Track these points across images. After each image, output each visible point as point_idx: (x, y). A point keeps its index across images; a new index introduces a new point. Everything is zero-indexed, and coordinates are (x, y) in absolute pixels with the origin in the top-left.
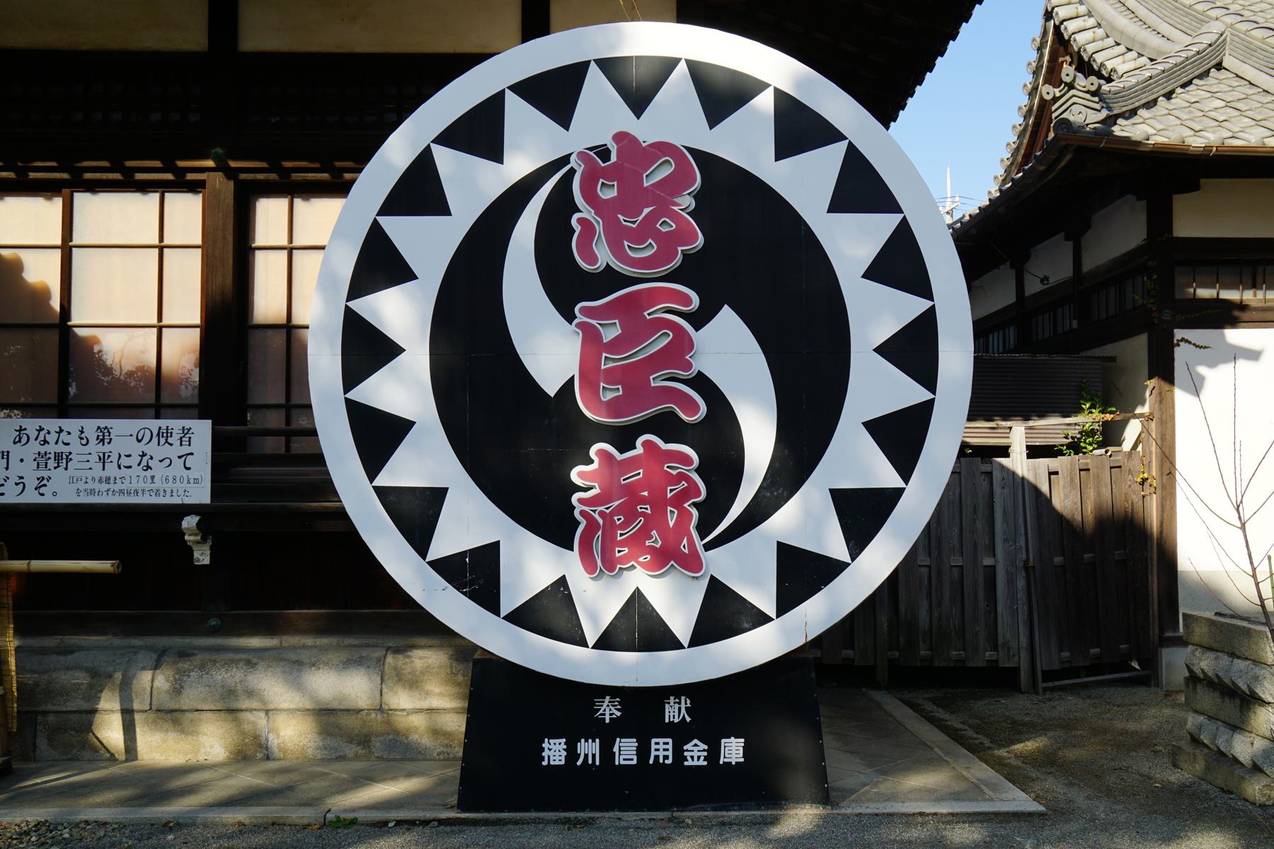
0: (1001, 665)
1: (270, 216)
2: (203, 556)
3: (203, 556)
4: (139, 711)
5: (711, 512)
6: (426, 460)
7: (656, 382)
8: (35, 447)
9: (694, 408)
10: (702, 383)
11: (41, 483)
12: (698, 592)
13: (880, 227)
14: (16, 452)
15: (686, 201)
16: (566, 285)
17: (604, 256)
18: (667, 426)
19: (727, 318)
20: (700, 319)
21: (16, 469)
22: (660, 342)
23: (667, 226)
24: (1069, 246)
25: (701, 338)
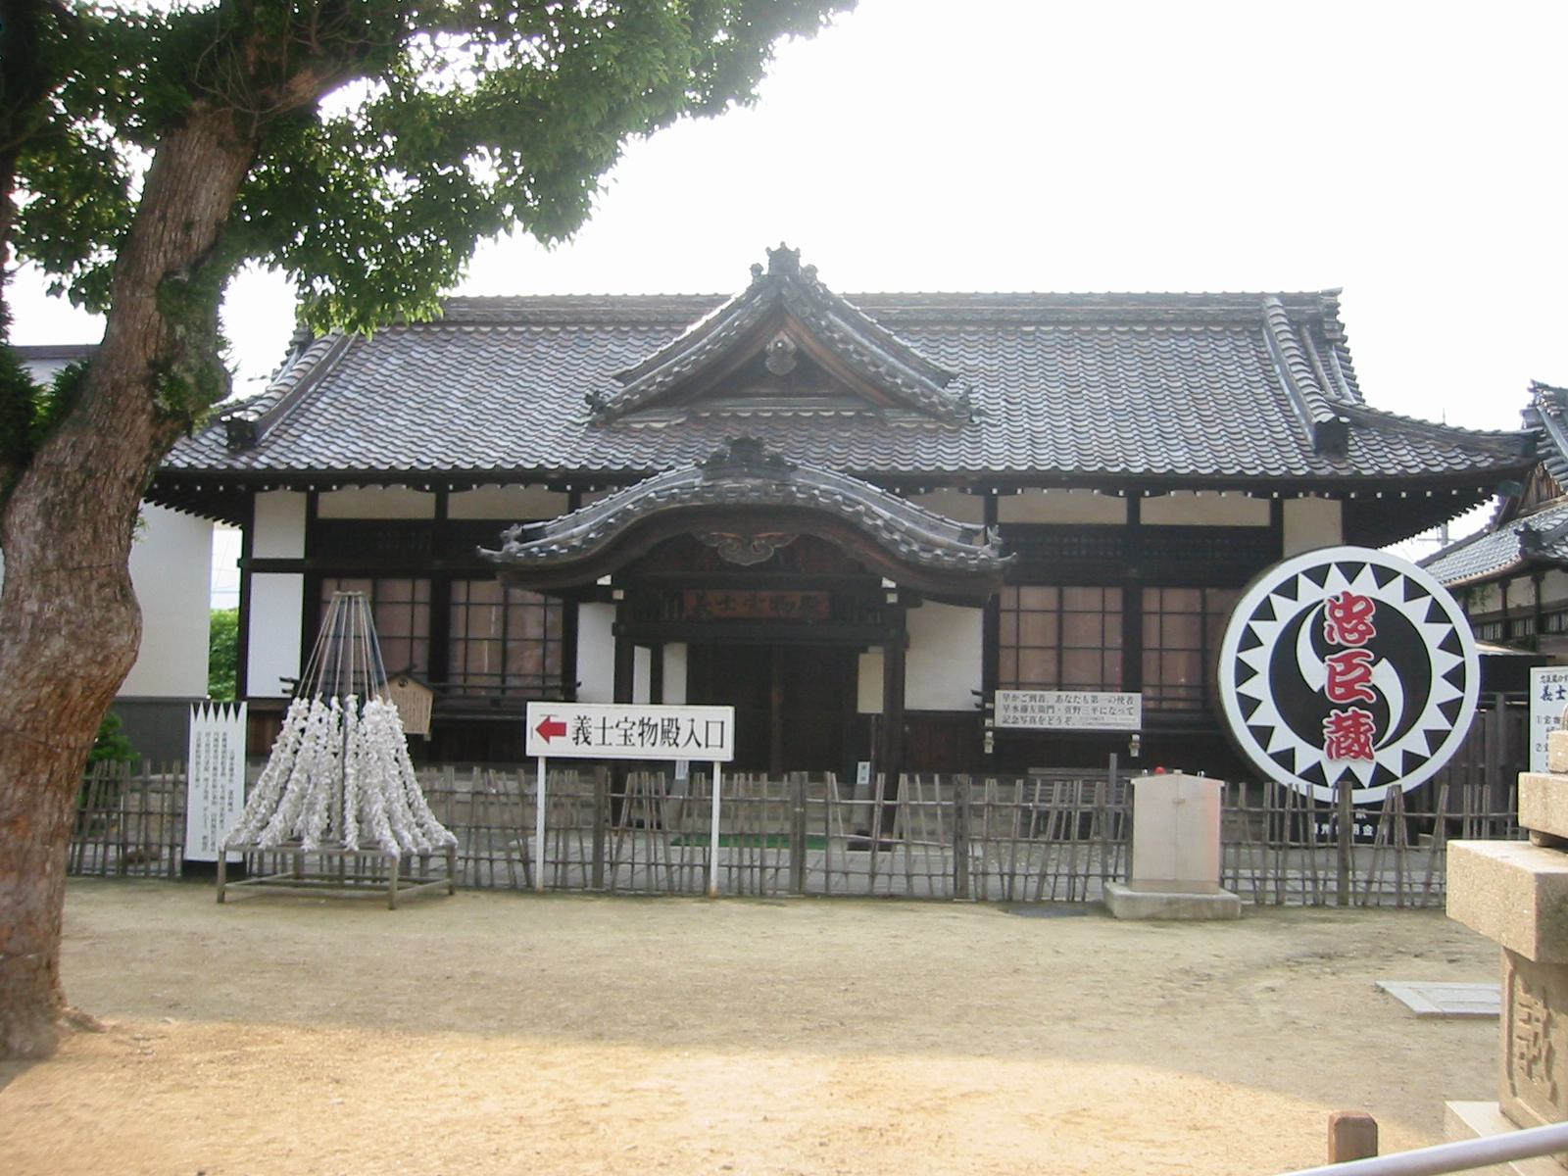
0: (1522, 776)
1: (1151, 599)
2: (989, 750)
3: (989, 750)
4: (873, 858)
5: (1377, 738)
6: (1268, 714)
7: (1357, 687)
8: (1066, 704)
9: (1371, 698)
10: (1374, 688)
11: (1068, 719)
12: (1373, 766)
13: (1399, 582)
14: (1057, 705)
15: (1369, 619)
16: (1322, 649)
17: (1337, 639)
18: (1361, 704)
19: (1384, 661)
20: (1374, 664)
21: (1057, 713)
22: (1358, 672)
23: (1361, 627)
24: (1500, 591)
25: (1373, 670)
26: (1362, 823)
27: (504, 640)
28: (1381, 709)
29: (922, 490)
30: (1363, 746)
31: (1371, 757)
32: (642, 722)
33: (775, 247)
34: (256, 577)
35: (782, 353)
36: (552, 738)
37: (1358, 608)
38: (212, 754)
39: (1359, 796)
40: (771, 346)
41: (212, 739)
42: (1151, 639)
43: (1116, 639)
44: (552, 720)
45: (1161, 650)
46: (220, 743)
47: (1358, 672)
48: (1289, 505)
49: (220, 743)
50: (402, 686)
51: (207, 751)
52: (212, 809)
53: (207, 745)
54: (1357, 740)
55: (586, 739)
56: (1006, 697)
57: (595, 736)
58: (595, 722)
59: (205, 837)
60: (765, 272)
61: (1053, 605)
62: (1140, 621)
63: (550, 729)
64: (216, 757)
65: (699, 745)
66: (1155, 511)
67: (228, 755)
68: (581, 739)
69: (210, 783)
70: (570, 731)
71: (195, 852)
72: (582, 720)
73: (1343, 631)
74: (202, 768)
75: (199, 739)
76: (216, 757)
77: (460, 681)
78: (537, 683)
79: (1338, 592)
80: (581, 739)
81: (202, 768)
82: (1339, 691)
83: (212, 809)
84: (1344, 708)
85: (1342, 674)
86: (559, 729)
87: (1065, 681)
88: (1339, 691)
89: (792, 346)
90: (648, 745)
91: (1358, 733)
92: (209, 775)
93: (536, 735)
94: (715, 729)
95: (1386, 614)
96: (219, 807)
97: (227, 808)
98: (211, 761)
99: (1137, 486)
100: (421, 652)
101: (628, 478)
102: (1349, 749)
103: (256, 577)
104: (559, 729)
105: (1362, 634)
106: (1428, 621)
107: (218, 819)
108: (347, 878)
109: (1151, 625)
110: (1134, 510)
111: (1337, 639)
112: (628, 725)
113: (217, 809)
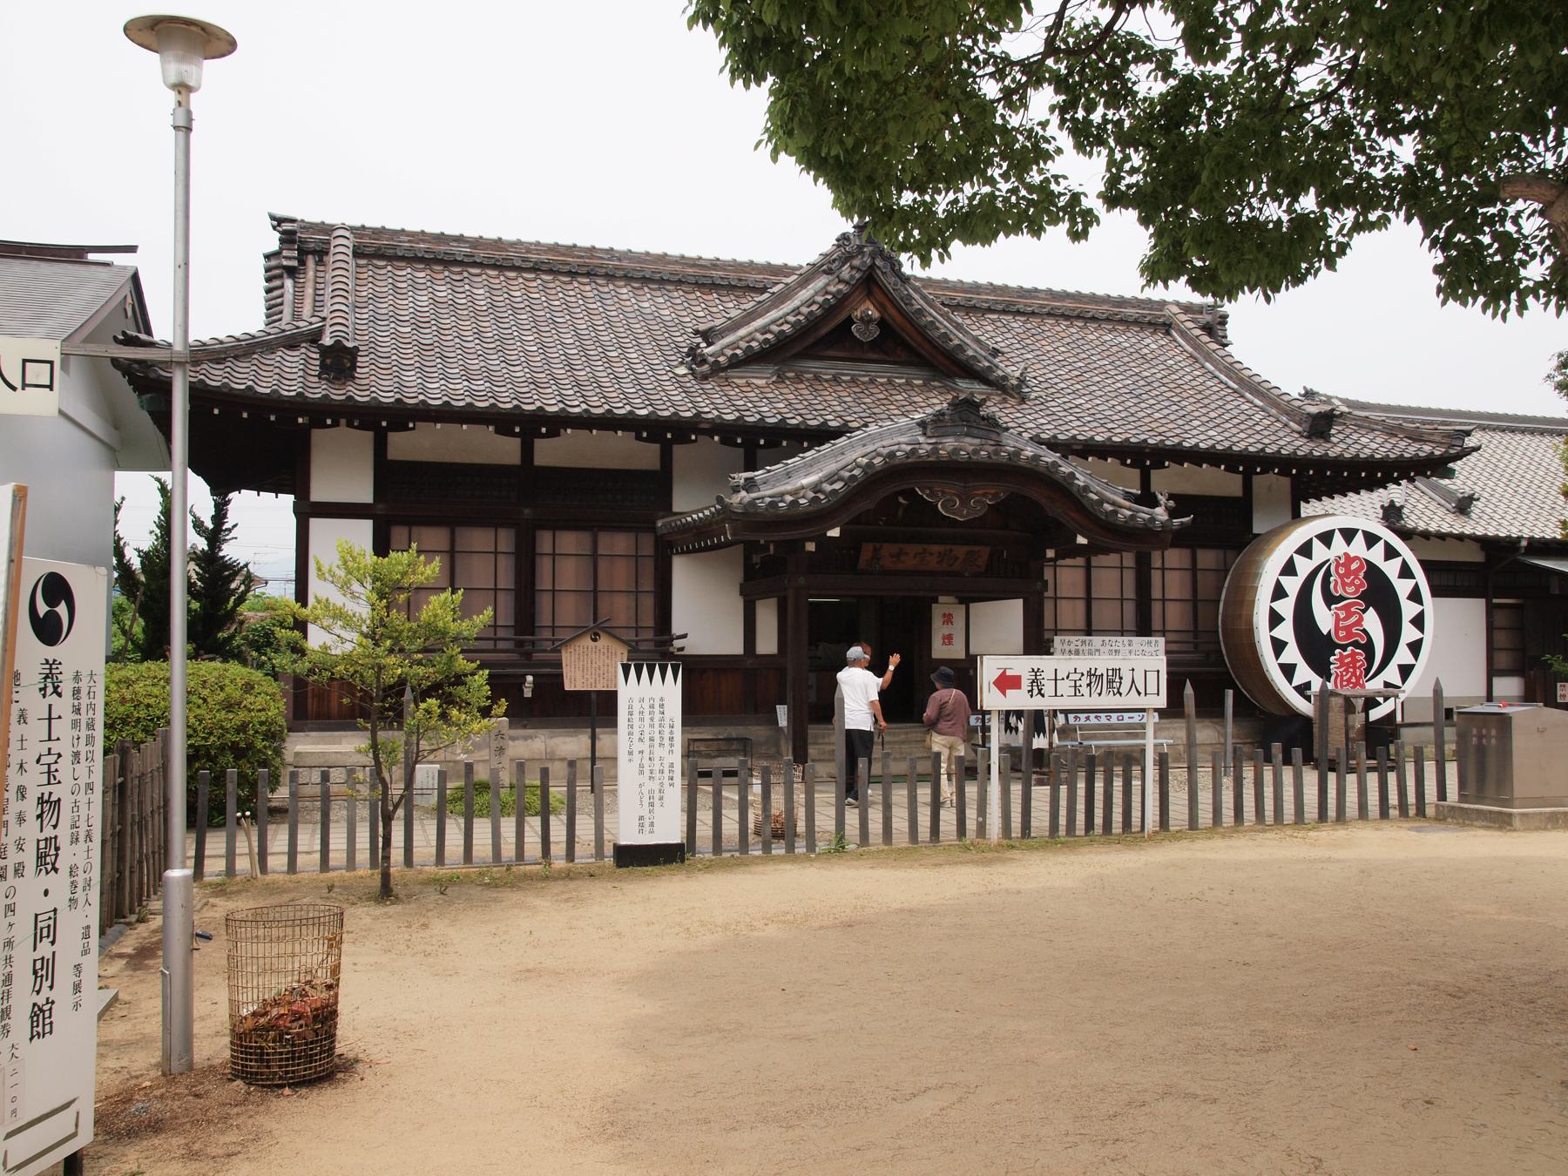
2: (528, 693)
3: (528, 693)
6: (1292, 654)
10: (1364, 631)
15: (1361, 575)
16: (1330, 599)
17: (1341, 591)
18: (1356, 644)
20: (1364, 611)
22: (1354, 619)
28: (1369, 648)
29: (329, 422)
30: (1358, 679)
34: (316, 524)
35: (867, 320)
37: (1354, 566)
40: (858, 313)
41: (646, 705)
42: (1156, 593)
43: (1130, 592)
44: (1009, 673)
45: (1164, 600)
46: (657, 709)
47: (1354, 619)
48: (678, 451)
49: (657, 709)
50: (595, 640)
51: (642, 720)
52: (650, 785)
53: (641, 713)
54: (1354, 674)
56: (1063, 642)
57: (1048, 688)
59: (641, 818)
61: (1187, 564)
63: (1007, 682)
64: (652, 726)
66: (548, 452)
67: (667, 723)
69: (646, 755)
70: (1025, 683)
72: (1036, 672)
73: (1344, 585)
74: (636, 736)
75: (630, 707)
76: (652, 726)
77: (547, 634)
79: (1340, 553)
83: (650, 785)
84: (1344, 648)
85: (1345, 619)
86: (1015, 682)
89: (877, 315)
90: (1095, 695)
91: (1355, 668)
92: (645, 746)
93: (994, 688)
94: (1152, 677)
95: (1373, 572)
97: (666, 782)
98: (647, 730)
99: (529, 425)
100: (1130, 608)
101: (823, 435)
102: (1349, 681)
103: (316, 524)
104: (1015, 682)
105: (1358, 587)
107: (657, 795)
110: (527, 451)
112: (1077, 676)
113: (656, 787)
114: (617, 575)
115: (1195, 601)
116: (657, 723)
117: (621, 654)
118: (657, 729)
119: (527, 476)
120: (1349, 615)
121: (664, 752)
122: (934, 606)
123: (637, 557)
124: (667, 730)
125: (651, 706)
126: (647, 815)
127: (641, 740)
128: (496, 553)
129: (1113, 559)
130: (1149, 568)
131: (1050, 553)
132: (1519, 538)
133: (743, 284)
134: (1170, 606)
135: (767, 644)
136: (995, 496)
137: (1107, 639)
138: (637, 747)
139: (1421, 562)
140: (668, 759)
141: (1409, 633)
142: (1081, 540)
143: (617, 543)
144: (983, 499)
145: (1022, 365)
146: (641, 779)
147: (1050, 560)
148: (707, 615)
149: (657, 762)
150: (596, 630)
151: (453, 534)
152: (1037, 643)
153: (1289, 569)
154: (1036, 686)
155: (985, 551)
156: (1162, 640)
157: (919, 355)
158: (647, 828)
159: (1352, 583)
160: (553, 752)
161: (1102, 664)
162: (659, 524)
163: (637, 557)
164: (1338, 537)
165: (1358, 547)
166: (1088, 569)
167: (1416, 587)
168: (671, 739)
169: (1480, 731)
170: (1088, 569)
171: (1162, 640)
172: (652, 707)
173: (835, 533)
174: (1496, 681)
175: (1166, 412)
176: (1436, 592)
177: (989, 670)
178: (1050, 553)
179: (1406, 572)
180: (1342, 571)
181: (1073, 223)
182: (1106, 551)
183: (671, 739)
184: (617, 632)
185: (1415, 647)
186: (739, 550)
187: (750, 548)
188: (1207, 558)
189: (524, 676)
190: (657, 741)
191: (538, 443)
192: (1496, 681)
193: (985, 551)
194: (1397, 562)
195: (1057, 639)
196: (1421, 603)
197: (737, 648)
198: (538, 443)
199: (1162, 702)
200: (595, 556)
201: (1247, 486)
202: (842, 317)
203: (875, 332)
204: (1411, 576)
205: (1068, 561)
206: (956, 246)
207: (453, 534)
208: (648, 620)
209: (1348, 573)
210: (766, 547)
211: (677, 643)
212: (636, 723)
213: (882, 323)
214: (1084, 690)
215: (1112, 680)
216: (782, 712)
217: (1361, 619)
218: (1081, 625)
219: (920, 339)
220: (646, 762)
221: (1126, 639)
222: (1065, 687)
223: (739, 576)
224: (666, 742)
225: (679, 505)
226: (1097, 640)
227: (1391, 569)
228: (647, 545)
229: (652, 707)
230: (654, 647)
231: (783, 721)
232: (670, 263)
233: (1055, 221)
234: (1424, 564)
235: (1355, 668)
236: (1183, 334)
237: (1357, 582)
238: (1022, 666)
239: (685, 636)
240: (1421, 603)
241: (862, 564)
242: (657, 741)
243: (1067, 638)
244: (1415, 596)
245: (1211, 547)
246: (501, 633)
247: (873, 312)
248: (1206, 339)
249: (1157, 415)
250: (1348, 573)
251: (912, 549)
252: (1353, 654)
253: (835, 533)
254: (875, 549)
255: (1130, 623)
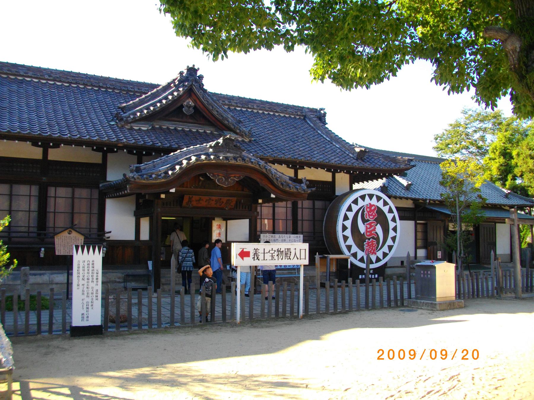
2: (42, 255)
3: (42, 255)
6: (350, 242)
10: (376, 233)
16: (364, 221)
17: (368, 218)
18: (373, 238)
20: (376, 225)
26: (372, 274)
27: (72, 213)
28: (378, 239)
30: (374, 251)
31: (376, 254)
32: (278, 251)
33: (191, 66)
35: (189, 107)
36: (244, 258)
37: (373, 208)
38: (86, 271)
39: (372, 266)
40: (185, 103)
41: (86, 263)
42: (299, 217)
44: (245, 250)
45: (302, 220)
46: (91, 266)
48: (110, 156)
49: (91, 266)
50: (69, 234)
51: (84, 270)
52: (87, 299)
53: (84, 267)
54: (372, 249)
55: (257, 258)
57: (261, 257)
58: (261, 251)
60: (184, 75)
61: (311, 207)
62: (46, 200)
64: (88, 273)
65: (298, 259)
66: (54, 155)
67: (95, 272)
68: (256, 258)
69: (86, 286)
70: (252, 255)
71: (77, 321)
72: (256, 250)
73: (369, 215)
74: (81, 278)
76: (88, 273)
78: (25, 229)
80: (256, 258)
81: (81, 278)
82: (368, 234)
83: (87, 299)
84: (369, 239)
85: (369, 228)
86: (247, 254)
87: (276, 230)
88: (368, 234)
89: (193, 104)
90: (280, 260)
92: (85, 282)
94: (303, 252)
95: (380, 212)
96: (90, 298)
97: (94, 298)
98: (86, 275)
100: (290, 223)
104: (247, 254)
105: (374, 216)
106: (352, 211)
107: (90, 304)
108: (179, 327)
109: (51, 202)
110: (45, 154)
111: (368, 218)
112: (273, 252)
113: (90, 300)
114: (82, 206)
115: (314, 220)
116: (90, 272)
117: (81, 239)
118: (90, 274)
119: (45, 164)
120: (371, 227)
121: (91, 285)
122: (213, 221)
123: (91, 199)
124: (95, 275)
125: (88, 263)
126: (85, 313)
127: (83, 279)
128: (30, 196)
129: (283, 204)
130: (297, 208)
131: (260, 201)
132: (426, 199)
133: (140, 91)
134: (304, 222)
135: (145, 236)
136: (239, 177)
137: (281, 235)
138: (81, 282)
139: (396, 207)
140: (96, 288)
141: (392, 234)
142: (273, 196)
143: (82, 193)
144: (235, 178)
145: (249, 128)
146: (83, 297)
147: (260, 204)
148: (120, 223)
149: (90, 289)
150: (72, 227)
151: (11, 187)
152: (254, 238)
153: (350, 209)
154: (256, 256)
155: (234, 199)
156: (302, 236)
157: (209, 121)
158: (85, 319)
159: (372, 215)
160: (52, 281)
161: (283, 246)
162: (101, 185)
163: (91, 199)
164: (367, 197)
165: (374, 201)
166: (274, 207)
167: (394, 216)
168: (97, 279)
169: (424, 272)
170: (274, 207)
171: (302, 236)
172: (88, 264)
173: (173, 190)
174: (418, 251)
175: (304, 148)
176: (401, 219)
177: (235, 249)
178: (260, 201)
179: (390, 211)
180: (368, 210)
181: (286, 43)
182: (281, 200)
183: (97, 279)
184: (77, 230)
185: (394, 239)
186: (134, 197)
187: (139, 196)
188: (319, 204)
189: (40, 249)
190: (91, 280)
191: (50, 150)
192: (418, 251)
193: (234, 199)
194: (388, 207)
195: (262, 235)
196: (396, 223)
197: (132, 237)
198: (50, 150)
199: (307, 262)
200: (73, 198)
201: (334, 177)
202: (179, 105)
203: (192, 111)
204: (393, 212)
205: (267, 204)
206: (229, 52)
207: (11, 187)
208: (95, 225)
209: (371, 211)
210: (145, 195)
211: (107, 235)
212: (81, 272)
213: (195, 108)
214: (276, 257)
215: (287, 253)
216: (150, 263)
217: (375, 228)
218: (271, 229)
219: (210, 115)
220: (85, 289)
221: (288, 235)
222: (268, 256)
223: (134, 208)
224: (95, 280)
225: (108, 179)
226: (277, 236)
227: (385, 209)
228: (96, 195)
229: (88, 264)
230: (95, 237)
231: (150, 268)
232: (110, 81)
233: (278, 43)
234: (398, 209)
235: (373, 247)
236: (310, 119)
237: (374, 214)
238: (250, 247)
239: (110, 232)
240: (396, 223)
241: (184, 204)
242: (91, 280)
243: (265, 235)
244: (394, 220)
245: (321, 200)
246: (31, 229)
247: (191, 103)
248: (318, 121)
249: (301, 149)
250: (371, 211)
251: (205, 198)
252: (372, 241)
253: (173, 190)
254: (190, 198)
255: (290, 229)
